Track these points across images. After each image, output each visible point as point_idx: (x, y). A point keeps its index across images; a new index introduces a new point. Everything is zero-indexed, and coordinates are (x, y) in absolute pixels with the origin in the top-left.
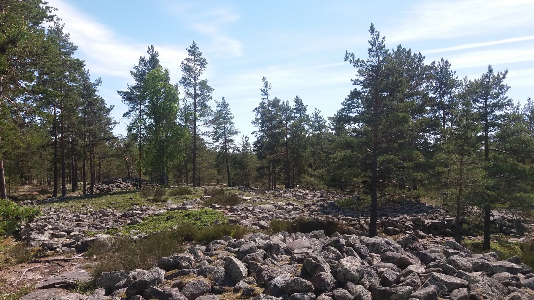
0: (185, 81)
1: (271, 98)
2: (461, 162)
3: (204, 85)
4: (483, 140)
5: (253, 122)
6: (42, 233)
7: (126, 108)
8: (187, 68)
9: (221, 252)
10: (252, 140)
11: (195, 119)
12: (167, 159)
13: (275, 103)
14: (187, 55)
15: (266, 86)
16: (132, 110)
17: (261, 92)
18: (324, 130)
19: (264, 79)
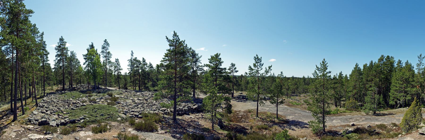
8: (103, 48)
13: (135, 59)
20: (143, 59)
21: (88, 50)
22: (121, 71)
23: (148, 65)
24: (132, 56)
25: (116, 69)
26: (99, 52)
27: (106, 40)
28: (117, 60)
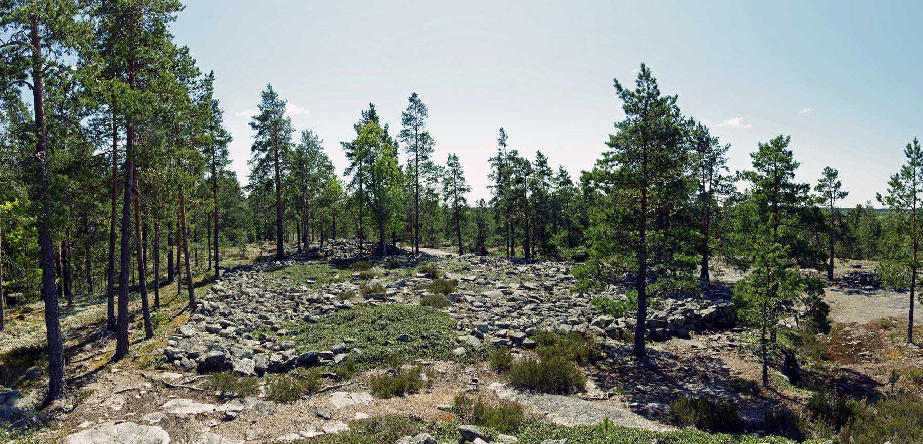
0: (405, 133)
1: (508, 150)
2: (182, 203)
3: (424, 137)
4: (513, 179)
5: (490, 176)
6: (307, 317)
7: (348, 164)
8: (407, 120)
9: (891, 310)
10: (488, 197)
11: (417, 175)
12: (78, 216)
13: (513, 157)
14: (408, 104)
15: (503, 136)
16: (354, 165)
17: (498, 142)
18: (569, 186)
19: (502, 130)
20: (540, 155)
21: (358, 128)
23: (555, 176)
24: (502, 147)
25: (450, 189)
26: (394, 133)
27: (414, 95)
28: (453, 160)
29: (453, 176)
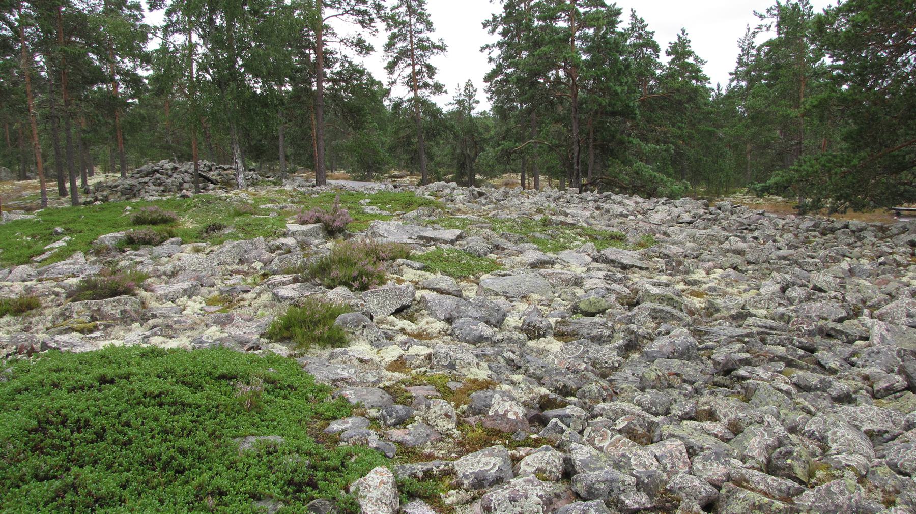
22: (434, 60)
29: (407, 19)
